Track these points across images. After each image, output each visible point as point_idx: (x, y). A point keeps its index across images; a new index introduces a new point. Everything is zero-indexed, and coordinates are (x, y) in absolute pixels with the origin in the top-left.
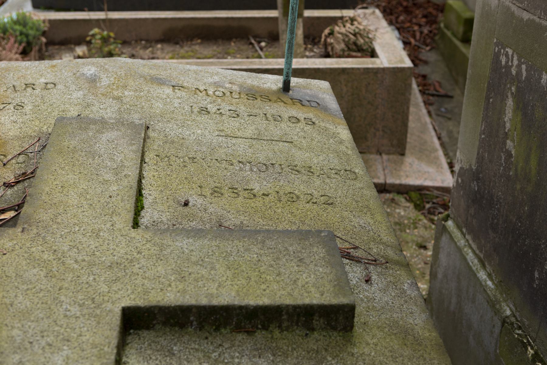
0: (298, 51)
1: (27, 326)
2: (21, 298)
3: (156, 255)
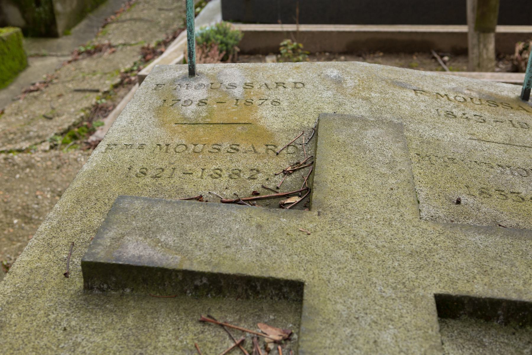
0: (490, 66)
1: (349, 302)
2: (335, 276)
3: (452, 247)
